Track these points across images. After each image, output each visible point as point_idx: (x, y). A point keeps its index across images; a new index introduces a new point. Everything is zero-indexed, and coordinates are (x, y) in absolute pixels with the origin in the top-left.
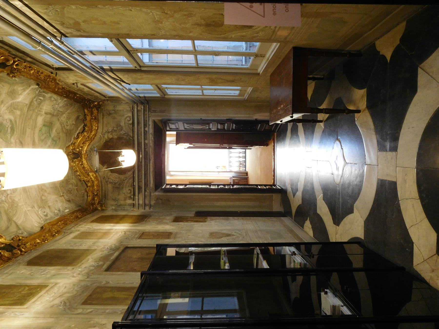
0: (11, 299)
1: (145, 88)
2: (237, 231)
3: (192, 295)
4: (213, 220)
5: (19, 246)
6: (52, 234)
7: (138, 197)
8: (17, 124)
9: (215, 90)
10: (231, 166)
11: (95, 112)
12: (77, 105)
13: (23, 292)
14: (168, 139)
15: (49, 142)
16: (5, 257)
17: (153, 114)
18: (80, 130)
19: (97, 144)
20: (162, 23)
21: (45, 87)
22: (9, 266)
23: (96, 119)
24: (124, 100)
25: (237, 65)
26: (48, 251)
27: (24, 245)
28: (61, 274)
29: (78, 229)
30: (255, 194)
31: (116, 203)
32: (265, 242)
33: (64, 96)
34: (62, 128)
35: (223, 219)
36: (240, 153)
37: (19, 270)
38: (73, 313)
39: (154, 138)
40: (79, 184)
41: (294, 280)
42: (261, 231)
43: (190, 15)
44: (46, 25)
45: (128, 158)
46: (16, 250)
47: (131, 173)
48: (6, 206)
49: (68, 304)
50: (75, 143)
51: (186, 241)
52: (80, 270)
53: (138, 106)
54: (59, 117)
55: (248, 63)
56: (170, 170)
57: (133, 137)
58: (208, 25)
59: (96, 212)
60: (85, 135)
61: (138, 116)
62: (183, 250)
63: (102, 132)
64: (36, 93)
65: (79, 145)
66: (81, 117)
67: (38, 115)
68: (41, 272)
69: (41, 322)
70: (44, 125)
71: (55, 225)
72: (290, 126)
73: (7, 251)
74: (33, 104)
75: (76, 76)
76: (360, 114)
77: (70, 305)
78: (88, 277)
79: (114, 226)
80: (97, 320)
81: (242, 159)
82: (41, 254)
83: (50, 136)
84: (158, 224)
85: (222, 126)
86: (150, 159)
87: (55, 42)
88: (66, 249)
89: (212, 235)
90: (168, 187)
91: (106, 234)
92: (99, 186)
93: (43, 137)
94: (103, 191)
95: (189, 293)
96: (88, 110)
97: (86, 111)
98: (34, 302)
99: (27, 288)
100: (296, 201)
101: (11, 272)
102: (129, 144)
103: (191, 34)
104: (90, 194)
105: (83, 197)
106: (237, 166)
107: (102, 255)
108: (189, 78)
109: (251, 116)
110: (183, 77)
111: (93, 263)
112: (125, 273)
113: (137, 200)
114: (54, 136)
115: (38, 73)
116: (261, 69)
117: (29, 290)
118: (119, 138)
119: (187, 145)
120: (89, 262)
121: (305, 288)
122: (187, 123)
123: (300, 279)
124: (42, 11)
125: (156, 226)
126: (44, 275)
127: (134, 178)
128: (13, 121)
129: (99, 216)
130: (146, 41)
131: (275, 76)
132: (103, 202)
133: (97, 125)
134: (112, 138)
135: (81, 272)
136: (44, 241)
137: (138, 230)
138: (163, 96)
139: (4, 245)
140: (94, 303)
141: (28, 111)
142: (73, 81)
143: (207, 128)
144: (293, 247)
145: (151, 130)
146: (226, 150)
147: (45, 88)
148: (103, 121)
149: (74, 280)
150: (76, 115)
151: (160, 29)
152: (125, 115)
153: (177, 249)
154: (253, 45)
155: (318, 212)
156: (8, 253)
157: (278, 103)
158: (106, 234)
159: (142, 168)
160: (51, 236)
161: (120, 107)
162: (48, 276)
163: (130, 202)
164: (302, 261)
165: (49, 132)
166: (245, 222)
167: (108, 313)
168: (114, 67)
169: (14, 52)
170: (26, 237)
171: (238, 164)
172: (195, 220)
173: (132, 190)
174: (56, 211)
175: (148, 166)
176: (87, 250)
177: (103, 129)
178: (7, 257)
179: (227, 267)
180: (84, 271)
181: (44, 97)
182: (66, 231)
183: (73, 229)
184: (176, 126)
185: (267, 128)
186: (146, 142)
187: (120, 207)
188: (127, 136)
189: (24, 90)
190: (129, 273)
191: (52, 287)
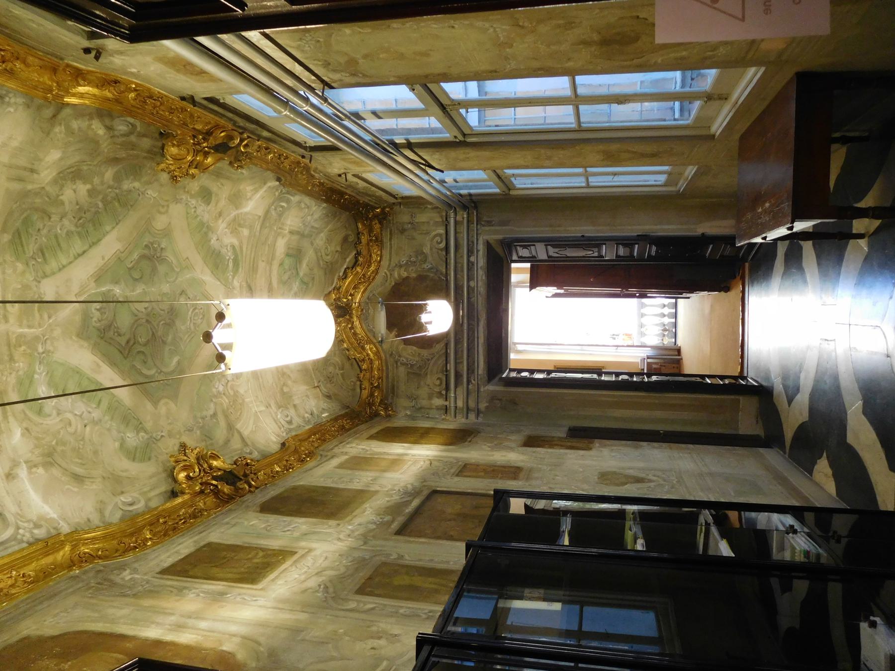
0: (235, 570)
1: (470, 177)
2: (660, 473)
3: (567, 598)
4: (605, 446)
5: (245, 475)
6: (300, 457)
7: (455, 393)
9: (615, 174)
10: (642, 334)
11: (377, 227)
12: (345, 215)
14: (514, 278)
15: (296, 286)
16: (224, 493)
17: (487, 228)
20: (511, 46)
21: (290, 184)
22: (230, 510)
23: (379, 241)
24: (431, 203)
25: (665, 120)
26: (295, 488)
27: (255, 474)
28: (314, 533)
29: (344, 450)
31: (413, 404)
32: (723, 500)
34: (318, 260)
35: (626, 446)
36: (664, 306)
37: (247, 520)
40: (347, 365)
41: (787, 588)
42: (711, 474)
43: (570, 25)
44: (298, 69)
45: (438, 317)
47: (442, 345)
48: (225, 401)
49: (331, 590)
51: (551, 486)
55: (686, 114)
56: (516, 341)
57: (447, 275)
58: (605, 42)
59: (377, 419)
61: (456, 233)
62: (541, 504)
63: (390, 264)
65: (347, 292)
66: (351, 238)
67: (278, 235)
68: (285, 527)
69: (286, 617)
70: (288, 255)
72: (782, 249)
75: (343, 159)
77: (334, 592)
78: (365, 543)
79: (410, 449)
80: (382, 625)
81: (667, 320)
82: (280, 494)
83: (298, 274)
84: (492, 449)
85: (628, 250)
86: (478, 319)
87: (314, 100)
89: (605, 477)
90: (513, 374)
91: (396, 462)
93: (286, 277)
95: (561, 593)
96: (363, 224)
97: (360, 226)
98: (273, 580)
99: (261, 554)
100: (795, 415)
101: (233, 522)
102: (438, 290)
103: (570, 64)
104: (366, 384)
105: (354, 390)
106: (658, 335)
107: (390, 504)
108: (561, 154)
110: (549, 152)
111: (373, 518)
112: (432, 541)
113: (452, 400)
114: (305, 275)
115: (279, 159)
116: (717, 127)
117: (264, 557)
118: (421, 278)
119: (553, 290)
121: (814, 606)
122: (554, 246)
123: (801, 587)
124: (293, 44)
127: (447, 355)
129: (380, 428)
130: (473, 85)
131: (751, 137)
132: (390, 400)
134: (407, 278)
135: (353, 531)
137: (456, 458)
142: (340, 169)
143: (596, 254)
144: (789, 516)
145: (481, 260)
146: (634, 301)
147: (291, 185)
149: (341, 546)
150: (343, 235)
151: (506, 58)
152: (430, 234)
153: (529, 502)
154: (703, 76)
155: (850, 439)
157: (757, 199)
158: (396, 462)
159: (463, 337)
161: (422, 217)
162: (296, 534)
163: (438, 402)
164: (812, 547)
165: (296, 268)
167: (405, 616)
168: (414, 139)
169: (241, 122)
170: (258, 461)
171: (658, 330)
173: (444, 379)
174: (306, 415)
175: (474, 332)
176: (361, 492)
177: (390, 260)
178: (228, 495)
179: (640, 545)
180: (357, 530)
181: (288, 201)
182: (325, 453)
183: (336, 450)
184: (531, 253)
185: (727, 253)
186: (472, 284)
189: (256, 190)
190: (441, 542)
191: (303, 556)
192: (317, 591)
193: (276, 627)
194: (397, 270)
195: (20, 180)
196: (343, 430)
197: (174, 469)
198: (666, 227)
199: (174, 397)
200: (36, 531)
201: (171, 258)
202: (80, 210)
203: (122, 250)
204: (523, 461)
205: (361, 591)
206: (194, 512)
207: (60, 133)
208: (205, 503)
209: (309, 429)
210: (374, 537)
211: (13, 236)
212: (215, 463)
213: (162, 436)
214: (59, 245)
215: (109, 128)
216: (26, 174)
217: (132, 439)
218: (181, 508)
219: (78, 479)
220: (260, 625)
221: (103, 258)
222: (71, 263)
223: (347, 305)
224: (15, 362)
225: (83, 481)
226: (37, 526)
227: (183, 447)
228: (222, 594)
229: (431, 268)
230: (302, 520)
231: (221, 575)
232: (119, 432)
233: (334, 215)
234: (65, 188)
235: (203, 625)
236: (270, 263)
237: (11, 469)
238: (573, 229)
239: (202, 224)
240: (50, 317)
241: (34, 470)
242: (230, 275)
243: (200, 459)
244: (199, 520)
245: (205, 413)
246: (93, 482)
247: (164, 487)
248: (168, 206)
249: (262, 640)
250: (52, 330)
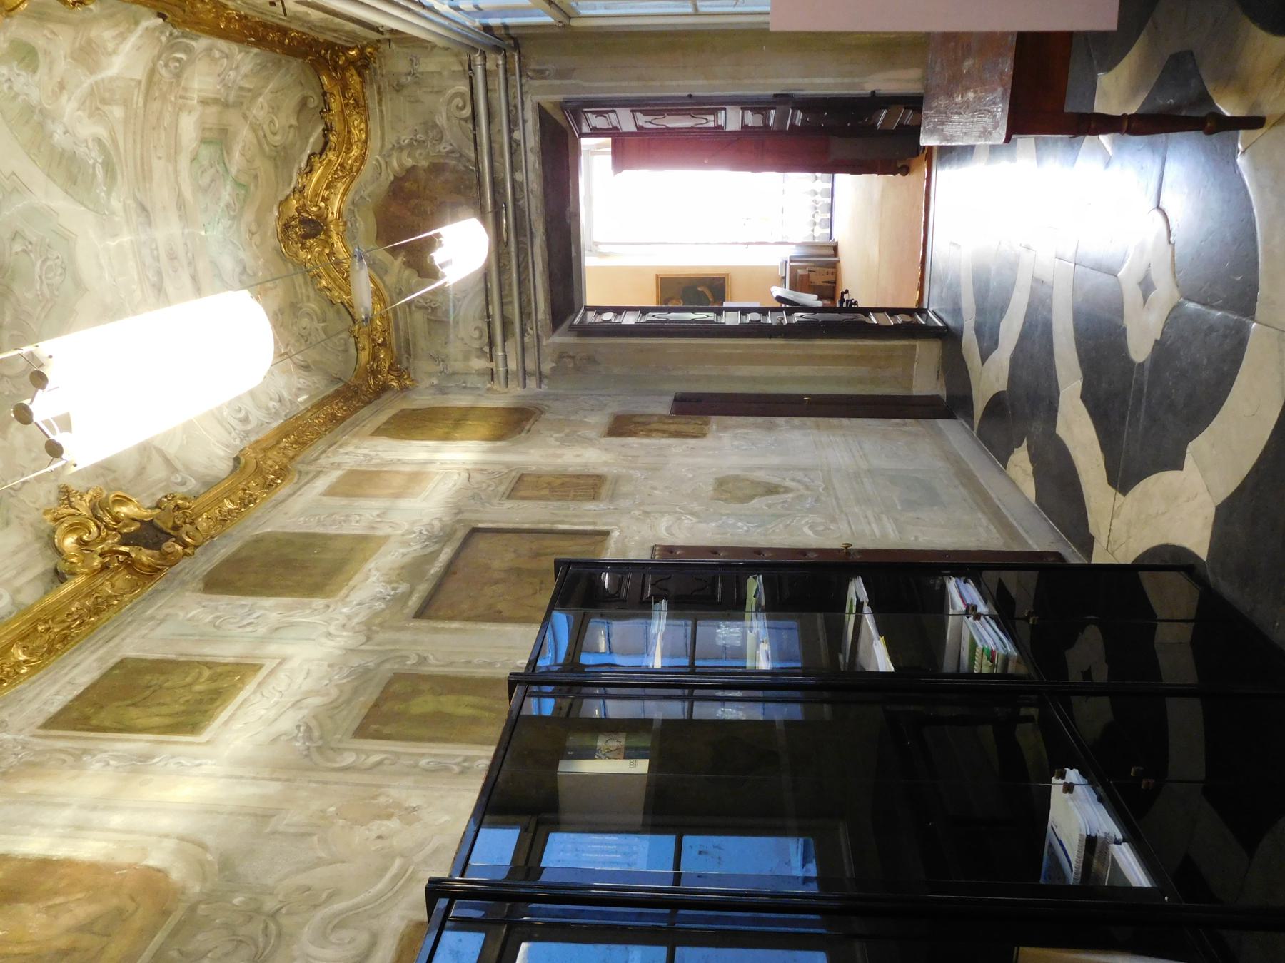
0: (165, 710)
2: (800, 475)
4: (725, 428)
8: (122, 150)
11: (354, 80)
12: (296, 63)
13: (198, 688)
16: (143, 564)
17: (537, 83)
18: (315, 143)
19: (370, 189)
21: (184, 22)
22: (156, 592)
23: (360, 106)
26: (258, 540)
28: (292, 625)
29: (336, 459)
30: (860, 342)
31: (441, 367)
33: (249, 42)
35: (757, 426)
38: (330, 765)
39: (544, 164)
40: (331, 313)
42: (871, 472)
46: (170, 543)
49: (316, 734)
50: (304, 187)
52: (345, 610)
53: (485, 59)
54: (244, 107)
56: (595, 239)
57: (477, 162)
59: (386, 396)
60: (330, 160)
61: (487, 91)
63: (382, 146)
64: (160, 41)
65: (316, 194)
66: (313, 102)
69: (249, 792)
70: (204, 141)
71: (272, 447)
73: (147, 547)
74: (156, 78)
76: (1259, 132)
77: (321, 738)
78: (368, 639)
79: (437, 450)
82: (239, 550)
83: (227, 170)
84: (562, 442)
86: (532, 233)
88: (307, 535)
91: (416, 478)
92: (388, 318)
93: (205, 180)
94: (402, 333)
96: (331, 78)
97: (325, 80)
98: (226, 723)
100: (991, 377)
101: (160, 615)
104: (364, 342)
105: (346, 351)
107: (407, 559)
109: (857, 80)
112: (470, 626)
113: (500, 360)
114: (239, 171)
117: (212, 679)
118: (436, 169)
120: (370, 584)
122: (646, 113)
125: (558, 452)
126: (249, 629)
128: (108, 143)
132: (405, 364)
133: (363, 126)
134: (414, 167)
135: (349, 618)
136: (246, 506)
137: (507, 465)
138: (566, 21)
139: (138, 524)
140: (386, 731)
143: (712, 124)
145: (531, 137)
148: (381, 111)
152: (445, 98)
156: (149, 552)
158: (416, 478)
159: (510, 261)
160: (263, 487)
161: (429, 65)
162: (262, 630)
163: (480, 364)
166: (824, 438)
172: (673, 428)
175: (527, 254)
176: (363, 539)
178: (149, 566)
181: (188, 49)
183: (323, 461)
186: (519, 177)
187: (449, 382)
188: (459, 160)
189: (122, 37)
191: (272, 672)
192: (295, 738)
193: (231, 813)
194: (395, 154)
196: (334, 421)
197: (54, 532)
198: (817, 81)
204: (606, 464)
205: (362, 732)
206: (95, 605)
208: (112, 586)
209: (278, 428)
210: (381, 625)
212: (123, 510)
218: (71, 603)
220: (206, 812)
223: (318, 217)
228: (145, 758)
229: (453, 152)
230: (271, 601)
231: (143, 722)
233: (278, 65)
235: (116, 820)
236: (173, 157)
238: (674, 83)
239: (29, 109)
242: (101, 192)
243: (98, 507)
244: (105, 615)
247: (41, 565)
249: (209, 840)
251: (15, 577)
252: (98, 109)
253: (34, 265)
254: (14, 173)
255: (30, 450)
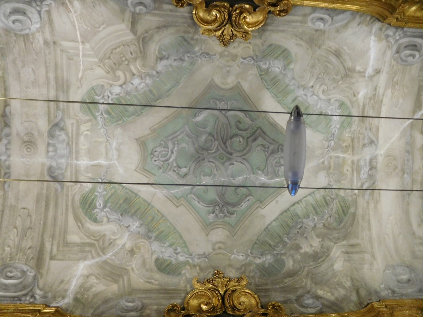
141: (42, 245)
189: (83, 288)
195: (352, 246)
199: (211, 86)
200: (391, 34)
201: (201, 207)
202: (302, 233)
203: (259, 209)
207: (345, 282)
211: (348, 211)
213: (244, 59)
214: (314, 208)
215: (317, 297)
216: (350, 250)
217: (276, 66)
219: (338, 54)
221: (277, 202)
222: (305, 197)
224: (351, 137)
225: (336, 51)
226: (387, 36)
227: (225, 42)
232: (285, 75)
234: (320, 246)
237: (374, 76)
240: (323, 162)
241: (362, 70)
245: (175, 64)
246: (330, 47)
248: (214, 249)
250: (322, 154)
251: (297, 21)
252: (97, 240)
253: (176, 160)
254: (177, 207)
255: (228, 72)
